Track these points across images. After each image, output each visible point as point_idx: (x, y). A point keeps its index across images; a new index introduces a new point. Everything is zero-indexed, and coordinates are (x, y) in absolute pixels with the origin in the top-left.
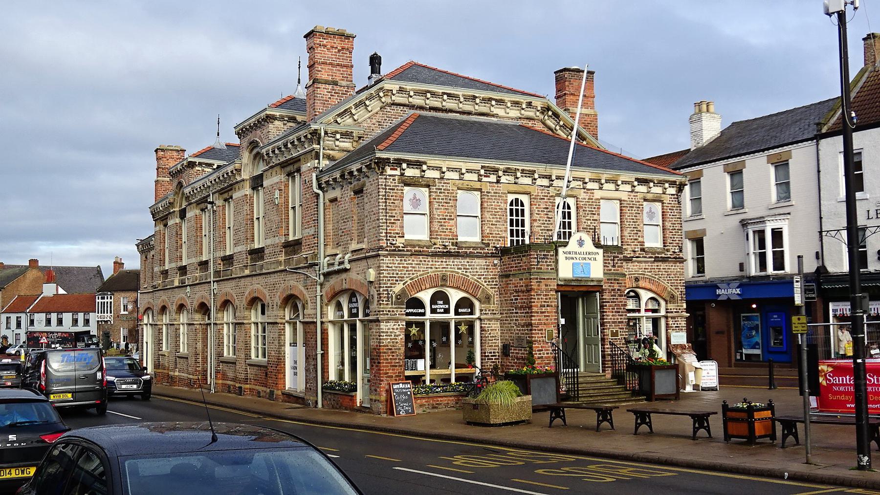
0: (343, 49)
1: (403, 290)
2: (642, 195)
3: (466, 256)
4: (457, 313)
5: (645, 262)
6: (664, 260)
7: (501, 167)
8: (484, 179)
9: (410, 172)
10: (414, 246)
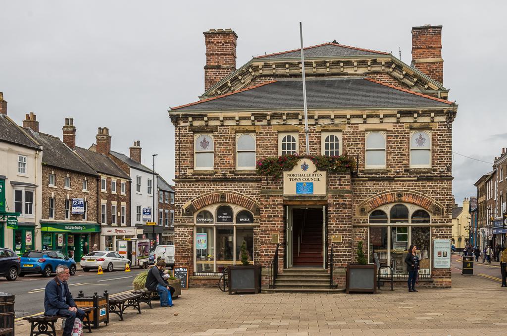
0: (226, 42)
1: (191, 206)
3: (240, 180)
4: (238, 221)
6: (429, 179)
7: (269, 113)
8: (257, 123)
9: (197, 123)
10: (372, 174)
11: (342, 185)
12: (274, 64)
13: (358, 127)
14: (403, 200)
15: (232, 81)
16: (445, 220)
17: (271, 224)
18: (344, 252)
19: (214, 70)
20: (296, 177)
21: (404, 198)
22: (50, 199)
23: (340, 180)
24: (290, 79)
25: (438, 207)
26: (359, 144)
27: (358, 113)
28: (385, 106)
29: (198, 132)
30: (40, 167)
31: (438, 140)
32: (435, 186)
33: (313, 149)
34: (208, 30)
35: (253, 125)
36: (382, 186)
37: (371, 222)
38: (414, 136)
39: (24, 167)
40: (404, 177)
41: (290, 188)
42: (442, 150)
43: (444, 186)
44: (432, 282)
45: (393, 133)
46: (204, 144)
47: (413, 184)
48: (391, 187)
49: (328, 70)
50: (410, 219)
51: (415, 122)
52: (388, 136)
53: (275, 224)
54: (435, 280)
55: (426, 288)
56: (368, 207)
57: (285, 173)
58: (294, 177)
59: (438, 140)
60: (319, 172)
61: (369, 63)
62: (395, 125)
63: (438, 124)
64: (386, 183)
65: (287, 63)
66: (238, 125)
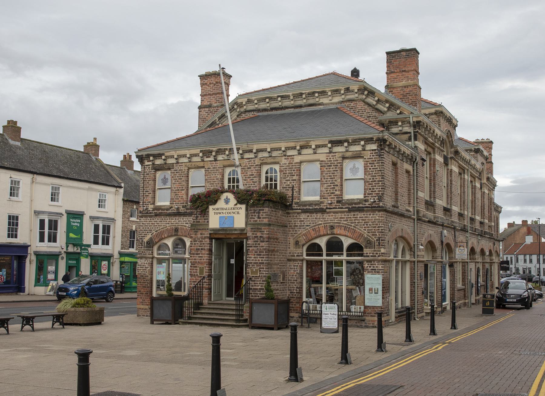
1: (151, 239)
2: (341, 155)
5: (341, 212)
6: (361, 210)
7: (214, 149)
8: (206, 159)
9: (158, 162)
10: (305, 205)
11: (260, 218)
12: (256, 99)
13: (293, 159)
14: (335, 232)
15: (220, 118)
16: (377, 254)
17: (199, 257)
18: (261, 286)
19: (206, 109)
20: (219, 211)
21: (336, 231)
22: (131, 232)
23: (259, 213)
24: (270, 113)
25: (369, 240)
26: (294, 175)
27: (292, 144)
28: (258, 141)
29: (159, 170)
30: (121, 203)
31: (370, 169)
32: (367, 217)
33: (253, 182)
34: (203, 73)
35: (203, 161)
36: (316, 218)
37: (307, 255)
38: (348, 165)
39: (105, 202)
40: (336, 208)
41: (214, 221)
42: (373, 179)
43: (375, 217)
44: (364, 320)
45: (326, 164)
46: (165, 181)
47: (345, 215)
48: (324, 218)
49: (305, 101)
50: (345, 253)
51: (347, 151)
52: (321, 166)
53: (202, 257)
54: (367, 318)
55: (358, 327)
56: (302, 240)
57: (211, 207)
58: (218, 211)
59: (370, 169)
60: (239, 206)
61: (342, 92)
62: (328, 155)
63: (369, 152)
64: (319, 215)
65: (267, 98)
66: (190, 162)
